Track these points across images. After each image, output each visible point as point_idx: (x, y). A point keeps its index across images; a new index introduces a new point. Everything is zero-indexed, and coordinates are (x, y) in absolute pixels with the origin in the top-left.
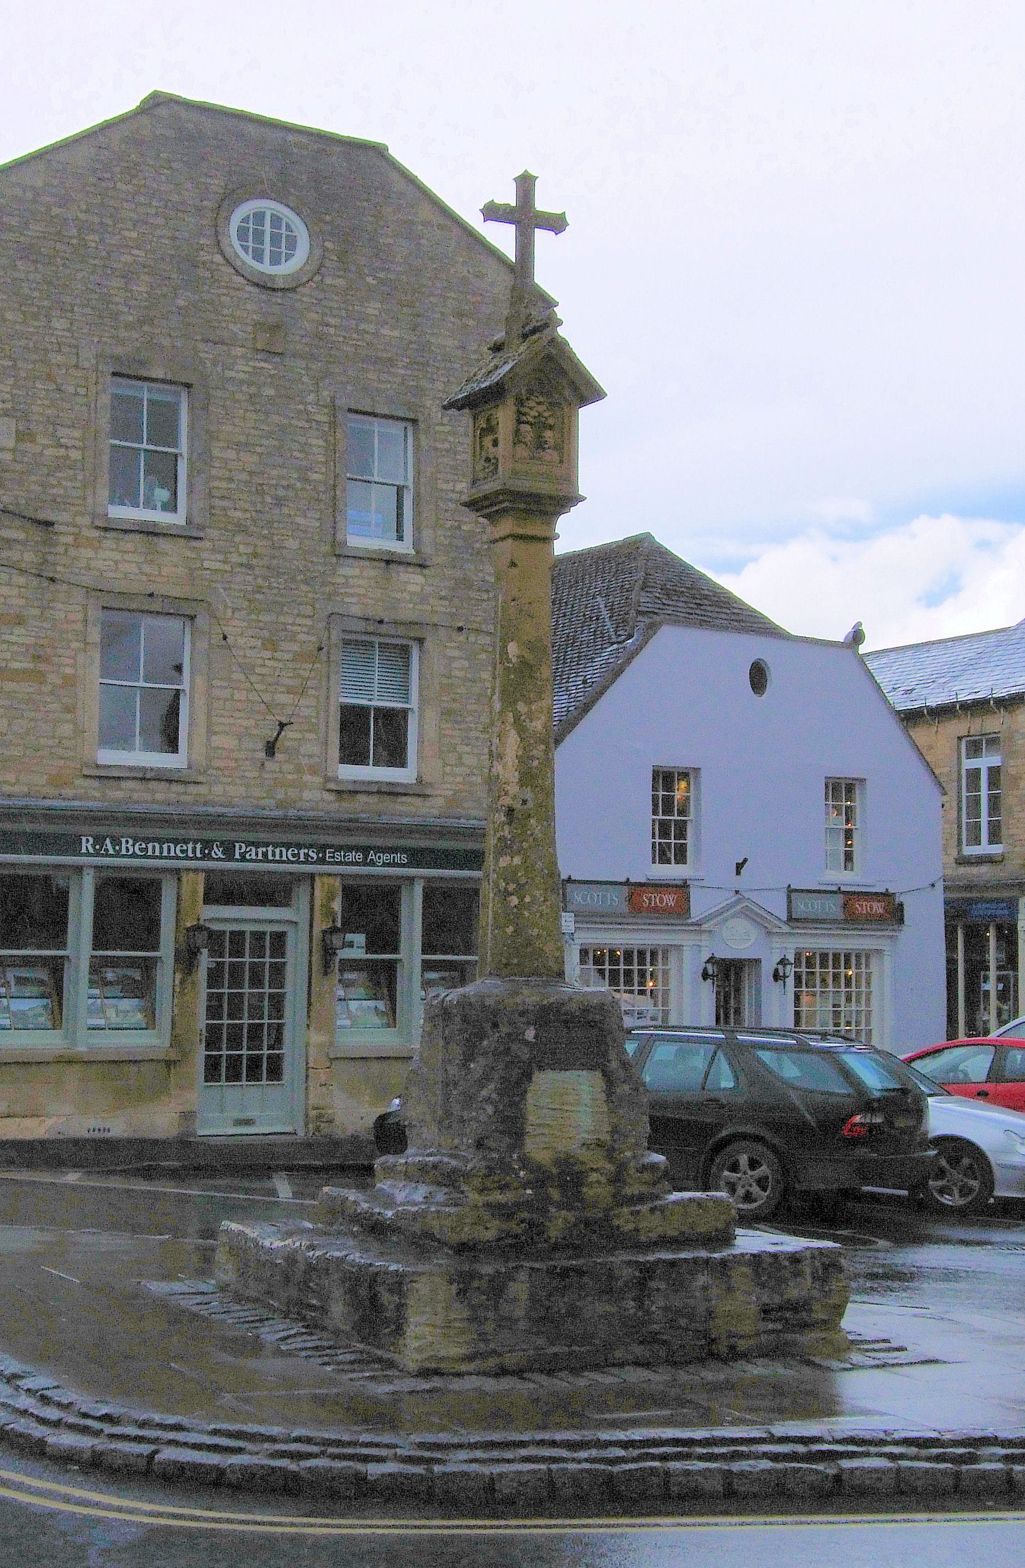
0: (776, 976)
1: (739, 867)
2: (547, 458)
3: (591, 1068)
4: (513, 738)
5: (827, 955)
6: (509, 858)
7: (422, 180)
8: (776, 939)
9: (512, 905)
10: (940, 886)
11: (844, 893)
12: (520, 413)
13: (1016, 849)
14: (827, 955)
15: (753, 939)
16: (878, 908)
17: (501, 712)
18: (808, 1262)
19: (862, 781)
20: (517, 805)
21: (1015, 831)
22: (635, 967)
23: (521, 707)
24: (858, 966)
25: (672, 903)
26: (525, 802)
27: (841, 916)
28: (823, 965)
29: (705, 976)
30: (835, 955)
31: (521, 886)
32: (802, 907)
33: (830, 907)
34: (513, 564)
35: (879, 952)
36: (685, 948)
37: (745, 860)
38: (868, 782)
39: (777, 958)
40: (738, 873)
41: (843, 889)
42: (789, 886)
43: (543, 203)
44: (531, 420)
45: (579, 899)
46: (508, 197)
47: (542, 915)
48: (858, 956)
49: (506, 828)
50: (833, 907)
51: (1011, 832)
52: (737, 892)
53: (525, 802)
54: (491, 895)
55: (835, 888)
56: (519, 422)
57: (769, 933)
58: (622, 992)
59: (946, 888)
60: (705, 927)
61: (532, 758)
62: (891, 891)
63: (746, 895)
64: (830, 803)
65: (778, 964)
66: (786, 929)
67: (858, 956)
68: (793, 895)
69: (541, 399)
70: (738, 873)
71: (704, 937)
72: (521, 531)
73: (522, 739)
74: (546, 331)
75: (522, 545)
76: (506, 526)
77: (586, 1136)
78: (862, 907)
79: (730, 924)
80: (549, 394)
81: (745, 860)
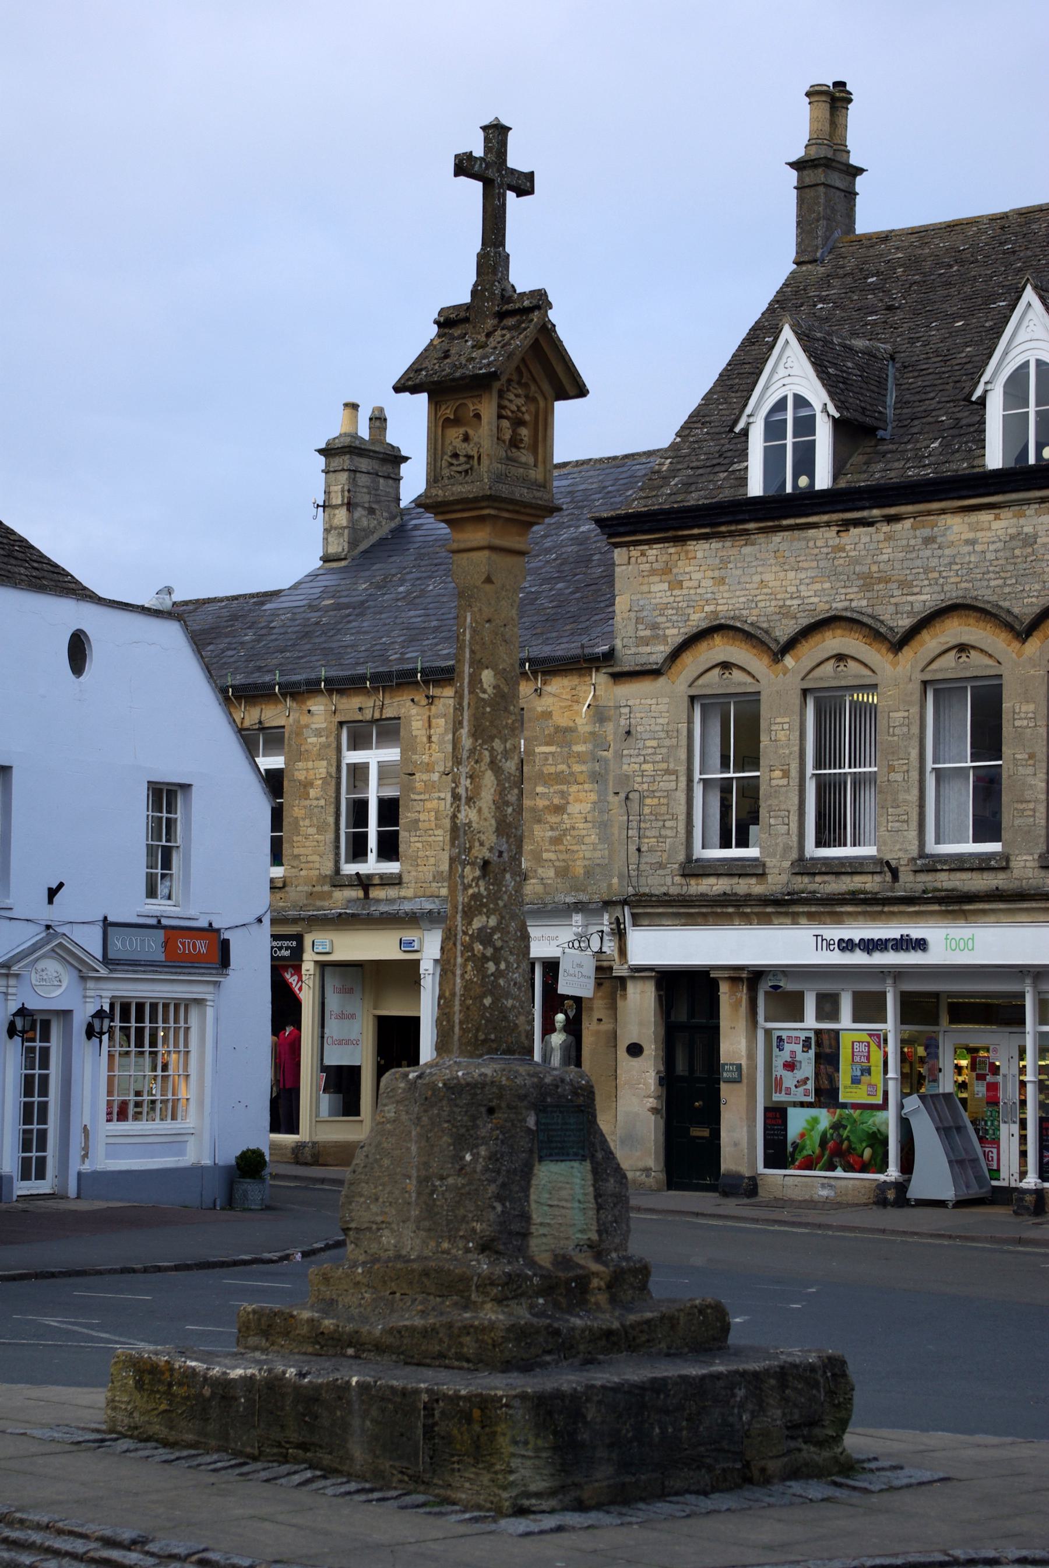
0: (90, 1032)
1: (52, 893)
2: (523, 459)
3: (583, 1159)
4: (489, 779)
5: (128, 1005)
6: (484, 918)
7: (901, 227)
8: (90, 984)
9: (489, 972)
10: (267, 920)
11: (165, 927)
12: (501, 407)
13: (302, 873)
14: (128, 1005)
15: (65, 984)
16: (202, 946)
17: (472, 751)
18: (820, 1372)
19: (186, 787)
20: (494, 858)
21: (302, 851)
22: (133, 1024)
23: (497, 744)
24: (165, 1020)
25: (204, 950)
26: (501, 854)
27: (161, 957)
28: (140, 1018)
29: (12, 1031)
30: (151, 1005)
31: (497, 950)
32: (120, 946)
33: (150, 946)
34: (489, 580)
35: (200, 1002)
36: (208, 1003)
37: (61, 885)
38: (194, 789)
39: (92, 1009)
40: (50, 901)
41: (164, 922)
42: (105, 918)
43: (516, 160)
44: (510, 414)
45: (119, 945)
46: (516, 160)
47: (515, 984)
48: (166, 1006)
49: (481, 883)
50: (152, 946)
51: (296, 851)
52: (48, 927)
53: (501, 854)
54: (459, 960)
55: (153, 921)
56: (500, 417)
57: (83, 978)
58: (133, 1055)
59: (274, 922)
60: (15, 969)
61: (507, 804)
62: (215, 926)
63: (59, 930)
64: (150, 813)
65: (93, 1016)
66: (103, 972)
67: (177, 1007)
68: (110, 929)
69: (520, 391)
70: (50, 901)
71: (12, 982)
72: (498, 542)
73: (499, 781)
74: (535, 316)
75: (498, 559)
76: (479, 536)
77: (579, 1236)
78: (184, 945)
79: (40, 965)
80: (526, 386)
81: (61, 885)
